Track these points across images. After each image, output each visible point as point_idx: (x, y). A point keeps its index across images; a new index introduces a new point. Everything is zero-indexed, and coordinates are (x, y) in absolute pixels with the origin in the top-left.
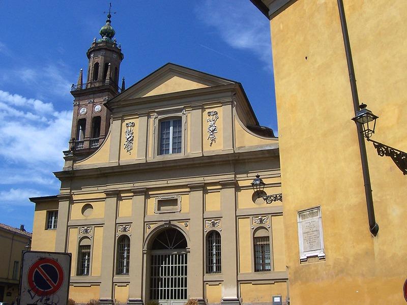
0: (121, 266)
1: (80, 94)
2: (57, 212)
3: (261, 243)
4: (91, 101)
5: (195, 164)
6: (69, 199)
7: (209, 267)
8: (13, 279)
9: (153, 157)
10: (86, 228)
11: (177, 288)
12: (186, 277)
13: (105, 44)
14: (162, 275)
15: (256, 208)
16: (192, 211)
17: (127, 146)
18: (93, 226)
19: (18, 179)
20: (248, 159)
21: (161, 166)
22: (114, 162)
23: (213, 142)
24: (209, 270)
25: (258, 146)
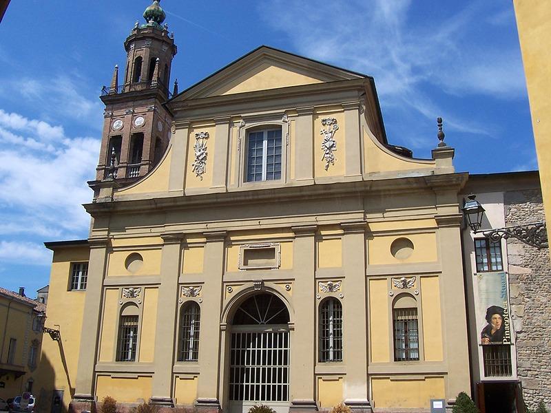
0: (186, 348)
1: (114, 100)
2: (86, 266)
3: (403, 318)
4: (130, 111)
5: (303, 196)
6: (106, 244)
7: (324, 353)
8: (8, 363)
9: (237, 184)
10: (132, 289)
11: (266, 384)
12: (285, 366)
13: (151, 31)
14: (248, 363)
15: (398, 265)
16: (299, 267)
17: (197, 168)
18: (143, 287)
19: (12, 228)
20: (385, 190)
21: (251, 198)
22: (176, 191)
23: (331, 164)
24: (324, 357)
25: (399, 172)
